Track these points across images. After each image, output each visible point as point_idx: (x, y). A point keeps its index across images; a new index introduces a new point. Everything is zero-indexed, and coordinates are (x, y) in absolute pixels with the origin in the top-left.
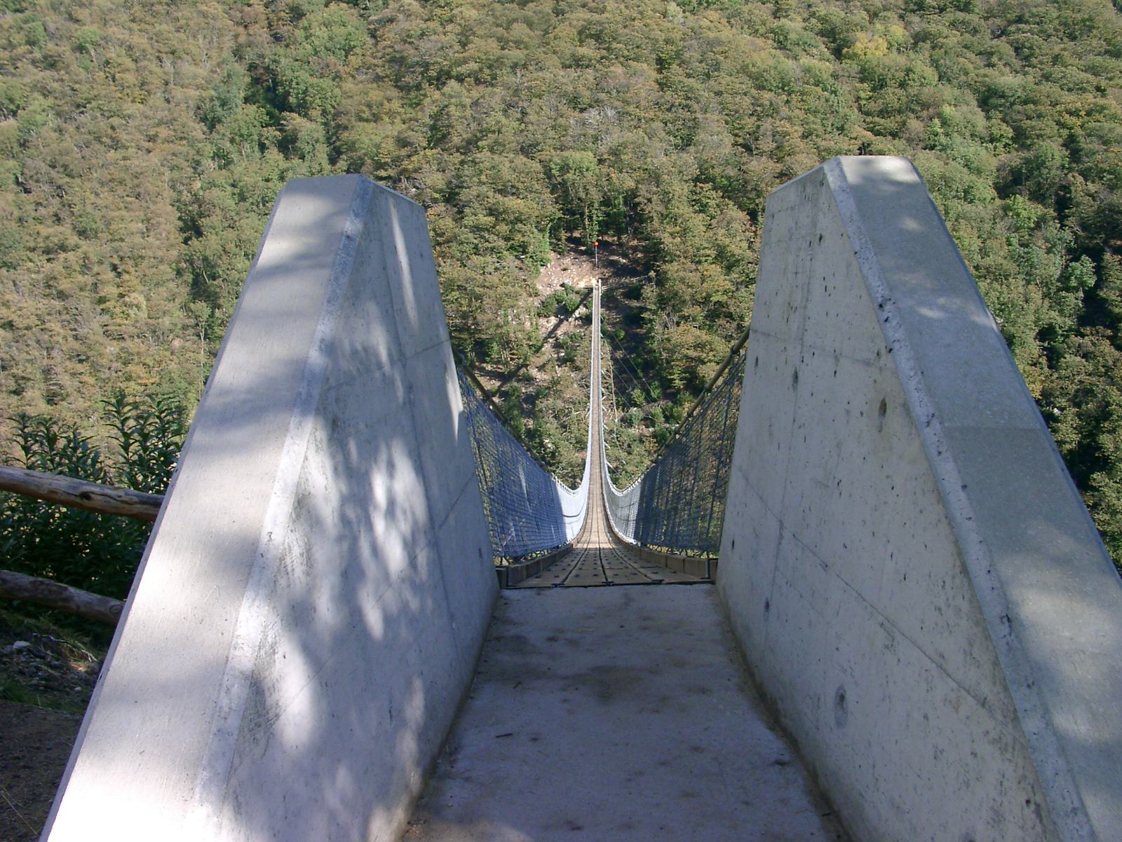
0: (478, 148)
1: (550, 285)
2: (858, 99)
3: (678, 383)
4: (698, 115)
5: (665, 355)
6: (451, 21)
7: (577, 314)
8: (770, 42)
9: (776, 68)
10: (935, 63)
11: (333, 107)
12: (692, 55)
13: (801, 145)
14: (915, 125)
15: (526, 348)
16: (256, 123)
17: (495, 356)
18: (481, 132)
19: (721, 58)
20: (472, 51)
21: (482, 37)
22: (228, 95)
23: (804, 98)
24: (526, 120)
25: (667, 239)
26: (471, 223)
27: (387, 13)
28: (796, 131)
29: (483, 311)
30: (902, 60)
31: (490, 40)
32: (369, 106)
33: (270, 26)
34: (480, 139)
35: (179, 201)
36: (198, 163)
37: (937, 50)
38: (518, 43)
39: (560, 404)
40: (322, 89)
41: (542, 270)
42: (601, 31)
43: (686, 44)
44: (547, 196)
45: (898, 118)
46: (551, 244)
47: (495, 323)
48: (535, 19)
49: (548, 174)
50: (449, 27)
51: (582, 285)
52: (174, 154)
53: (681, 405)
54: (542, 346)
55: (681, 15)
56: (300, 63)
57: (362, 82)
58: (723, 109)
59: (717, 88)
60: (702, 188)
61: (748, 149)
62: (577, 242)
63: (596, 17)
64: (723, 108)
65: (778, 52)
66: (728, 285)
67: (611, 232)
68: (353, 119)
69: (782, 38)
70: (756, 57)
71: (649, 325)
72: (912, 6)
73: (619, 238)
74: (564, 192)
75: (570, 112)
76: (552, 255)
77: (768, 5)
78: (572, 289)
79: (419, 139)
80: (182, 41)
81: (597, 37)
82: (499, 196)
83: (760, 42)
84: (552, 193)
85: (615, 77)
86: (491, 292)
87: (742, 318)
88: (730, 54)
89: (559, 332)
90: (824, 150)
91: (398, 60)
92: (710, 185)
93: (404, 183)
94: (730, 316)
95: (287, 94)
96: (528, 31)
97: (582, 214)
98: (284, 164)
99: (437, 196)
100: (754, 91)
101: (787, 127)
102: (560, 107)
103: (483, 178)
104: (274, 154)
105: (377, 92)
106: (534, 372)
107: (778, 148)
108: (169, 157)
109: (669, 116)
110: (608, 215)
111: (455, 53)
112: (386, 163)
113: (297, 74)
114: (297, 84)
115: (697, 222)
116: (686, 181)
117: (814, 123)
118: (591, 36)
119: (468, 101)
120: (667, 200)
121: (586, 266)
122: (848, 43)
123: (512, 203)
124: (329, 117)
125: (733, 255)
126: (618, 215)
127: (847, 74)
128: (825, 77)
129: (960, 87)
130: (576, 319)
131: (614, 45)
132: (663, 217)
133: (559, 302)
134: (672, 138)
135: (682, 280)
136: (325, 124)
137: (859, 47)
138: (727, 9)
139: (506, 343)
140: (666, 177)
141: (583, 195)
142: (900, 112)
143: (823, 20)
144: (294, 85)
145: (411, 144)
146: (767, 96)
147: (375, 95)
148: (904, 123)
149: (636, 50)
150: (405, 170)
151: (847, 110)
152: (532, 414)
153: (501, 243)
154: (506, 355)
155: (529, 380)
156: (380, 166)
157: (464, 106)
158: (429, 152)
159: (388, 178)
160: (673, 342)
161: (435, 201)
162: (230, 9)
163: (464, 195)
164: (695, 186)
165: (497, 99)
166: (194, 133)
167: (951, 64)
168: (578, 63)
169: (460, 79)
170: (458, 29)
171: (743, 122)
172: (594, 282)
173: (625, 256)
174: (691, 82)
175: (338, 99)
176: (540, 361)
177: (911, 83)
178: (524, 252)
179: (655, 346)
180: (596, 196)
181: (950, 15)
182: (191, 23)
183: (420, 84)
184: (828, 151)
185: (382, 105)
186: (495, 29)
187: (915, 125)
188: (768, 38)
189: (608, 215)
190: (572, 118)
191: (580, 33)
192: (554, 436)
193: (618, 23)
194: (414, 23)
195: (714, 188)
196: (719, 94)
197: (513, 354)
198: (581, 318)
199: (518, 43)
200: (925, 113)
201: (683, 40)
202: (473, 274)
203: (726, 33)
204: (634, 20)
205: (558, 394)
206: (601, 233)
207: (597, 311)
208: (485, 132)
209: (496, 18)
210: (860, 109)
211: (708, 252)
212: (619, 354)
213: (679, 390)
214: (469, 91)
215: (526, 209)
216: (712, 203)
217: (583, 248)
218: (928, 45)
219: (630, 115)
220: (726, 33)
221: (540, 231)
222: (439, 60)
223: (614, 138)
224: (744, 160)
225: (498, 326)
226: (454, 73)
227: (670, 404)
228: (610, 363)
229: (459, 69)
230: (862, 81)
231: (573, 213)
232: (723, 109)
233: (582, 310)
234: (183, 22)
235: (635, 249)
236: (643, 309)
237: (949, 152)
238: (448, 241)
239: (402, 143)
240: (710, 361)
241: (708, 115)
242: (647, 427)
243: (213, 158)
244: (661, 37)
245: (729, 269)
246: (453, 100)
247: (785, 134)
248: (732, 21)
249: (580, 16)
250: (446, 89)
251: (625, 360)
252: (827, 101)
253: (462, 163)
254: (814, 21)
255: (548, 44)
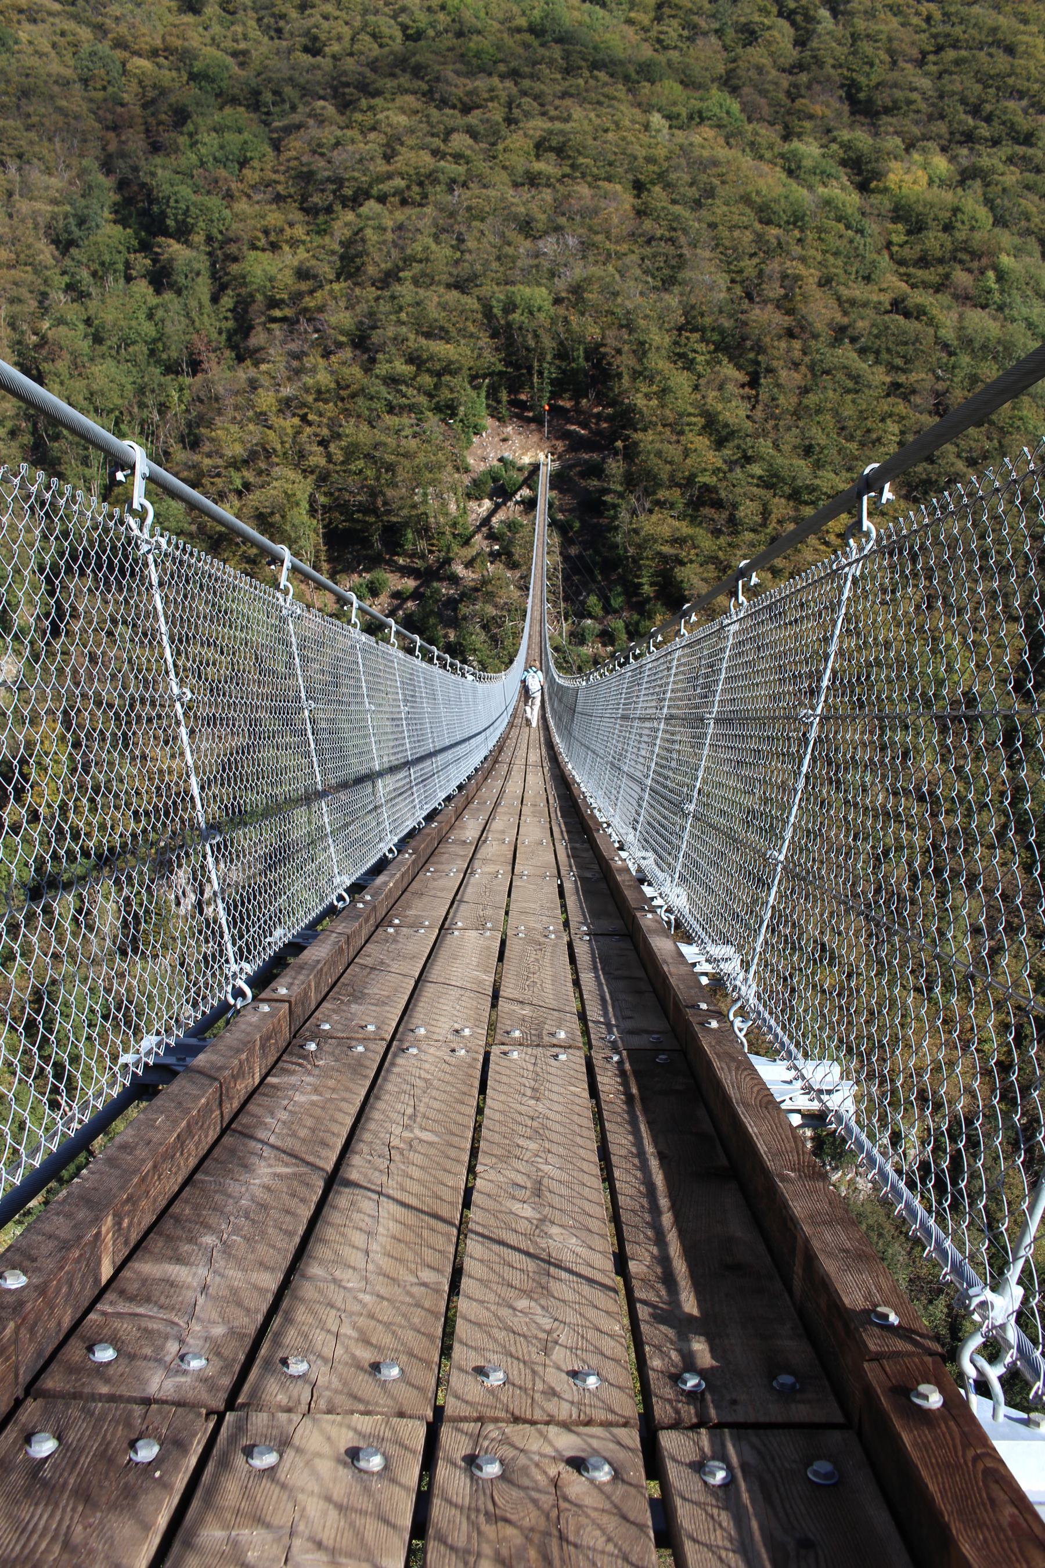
0: (399, 280)
1: (484, 459)
2: (889, 244)
3: (647, 589)
4: (685, 251)
5: (631, 551)
6: (374, 129)
7: (518, 497)
8: (778, 169)
9: (786, 197)
10: (989, 203)
11: (221, 232)
12: (681, 176)
13: (818, 294)
14: (961, 278)
15: (450, 537)
16: (121, 248)
17: (409, 547)
18: (405, 260)
19: (716, 182)
20: (399, 165)
21: (412, 148)
22: (86, 212)
23: (823, 235)
24: (463, 247)
25: (640, 401)
26: (384, 372)
27: (296, 118)
28: (811, 275)
29: (394, 485)
30: (948, 197)
31: (422, 152)
32: (266, 232)
33: (147, 131)
34: (403, 270)
35: (19, 342)
36: (44, 295)
37: (993, 186)
38: (458, 157)
39: (491, 611)
40: (208, 209)
41: (475, 439)
42: (564, 144)
43: (672, 163)
44: (485, 340)
45: (940, 270)
46: (488, 406)
47: (409, 502)
48: (481, 129)
49: (488, 312)
50: (372, 136)
51: (526, 460)
52: (16, 284)
53: (650, 618)
54: (472, 536)
55: (665, 131)
56: (180, 176)
57: (258, 202)
58: (717, 245)
59: (711, 219)
60: (688, 338)
61: (749, 296)
62: (522, 405)
63: (558, 125)
64: (717, 244)
65: (790, 181)
66: (719, 463)
67: (567, 395)
68: (245, 248)
69: (793, 166)
70: (761, 183)
71: (612, 512)
72: (958, 137)
73: (578, 403)
74: (507, 339)
75: (520, 238)
76: (489, 422)
77: (777, 127)
78: (512, 464)
79: (326, 269)
80: (31, 143)
81: (560, 151)
82: (423, 341)
83: (765, 168)
84: (492, 337)
85: (580, 199)
86: (406, 462)
87: (735, 506)
88: (731, 177)
89: (494, 520)
90: (846, 302)
91: (306, 177)
92: (697, 336)
93: (303, 325)
94: (718, 504)
95: (163, 215)
96: (470, 141)
97: (530, 368)
98: (153, 300)
99: (343, 339)
100: (758, 226)
101: (801, 269)
102: (507, 234)
103: (403, 316)
104: (142, 288)
105: (276, 215)
106: (459, 570)
107: (786, 296)
108: (8, 286)
109: (648, 251)
110: (564, 372)
111: (381, 167)
112: (282, 301)
113: (176, 188)
114: (177, 202)
115: (681, 380)
116: (668, 331)
117: (834, 266)
118: (551, 149)
119: (390, 224)
120: (641, 350)
121: (535, 438)
122: (878, 175)
123: (439, 348)
124: (216, 245)
125: (726, 425)
126: (575, 372)
127: (876, 212)
128: (849, 211)
129: (1020, 235)
130: (517, 503)
131: (581, 160)
132: (636, 375)
133: (495, 480)
134: (650, 279)
135: (659, 454)
136: (209, 254)
137: (892, 179)
138: (725, 126)
139: (424, 531)
140: (642, 322)
141: (532, 343)
142: (941, 261)
143: (847, 146)
144: (172, 203)
145: (315, 277)
146: (773, 232)
147: (274, 218)
148: (947, 276)
149: (608, 168)
150: (306, 310)
151: (875, 256)
152: (455, 623)
153: (423, 400)
154: (422, 545)
155: (454, 579)
156: (273, 303)
157: (385, 230)
158: (336, 286)
159: (284, 319)
160: (643, 533)
161: (340, 345)
162: (99, 108)
163: (376, 337)
164: (680, 335)
165: (427, 221)
166: (41, 257)
167: (1010, 205)
168: (533, 180)
169: (382, 199)
170: (382, 139)
171: (742, 264)
172: (541, 457)
173: (584, 425)
174: (677, 209)
175: (227, 223)
176: (469, 552)
177: (959, 225)
178: (453, 415)
179: (619, 539)
180: (548, 343)
181: (1007, 149)
182: (47, 122)
183: (330, 206)
184: (853, 302)
185: (282, 230)
186: (429, 139)
187: (961, 278)
188: (776, 165)
189: (564, 372)
190: (525, 246)
191: (538, 146)
192: (480, 651)
193: (585, 133)
194: (327, 130)
195: (703, 339)
196: (712, 226)
197: (433, 545)
198: (522, 502)
199: (458, 157)
200: (975, 265)
201: (668, 159)
202: (383, 438)
203: (723, 153)
204: (606, 131)
205: (490, 597)
206: (554, 395)
207: (544, 493)
208: (408, 261)
209: (432, 127)
210: (891, 257)
211: (693, 419)
212: (573, 551)
213: (648, 600)
214: (391, 212)
215: (456, 357)
216: (700, 359)
217: (531, 414)
218: (978, 184)
219: (598, 248)
220: (723, 153)
221: (474, 388)
222: (356, 174)
223: (577, 272)
224: (745, 307)
225: (414, 506)
226: (374, 191)
227: (636, 617)
228: (559, 559)
229: (381, 186)
230: (895, 220)
231: (517, 367)
232: (717, 245)
233: (525, 492)
234: (35, 119)
235: (598, 416)
236: (606, 491)
237: (1007, 311)
238: (353, 396)
239: (302, 274)
240: (691, 562)
241: (699, 251)
242: (604, 645)
243: (65, 292)
244: (641, 153)
245: (720, 444)
246: (370, 223)
247: (797, 278)
248: (732, 141)
249: (537, 126)
250: (364, 210)
251: (580, 557)
252: (851, 241)
253: (377, 299)
254: (834, 146)
255: (494, 157)
